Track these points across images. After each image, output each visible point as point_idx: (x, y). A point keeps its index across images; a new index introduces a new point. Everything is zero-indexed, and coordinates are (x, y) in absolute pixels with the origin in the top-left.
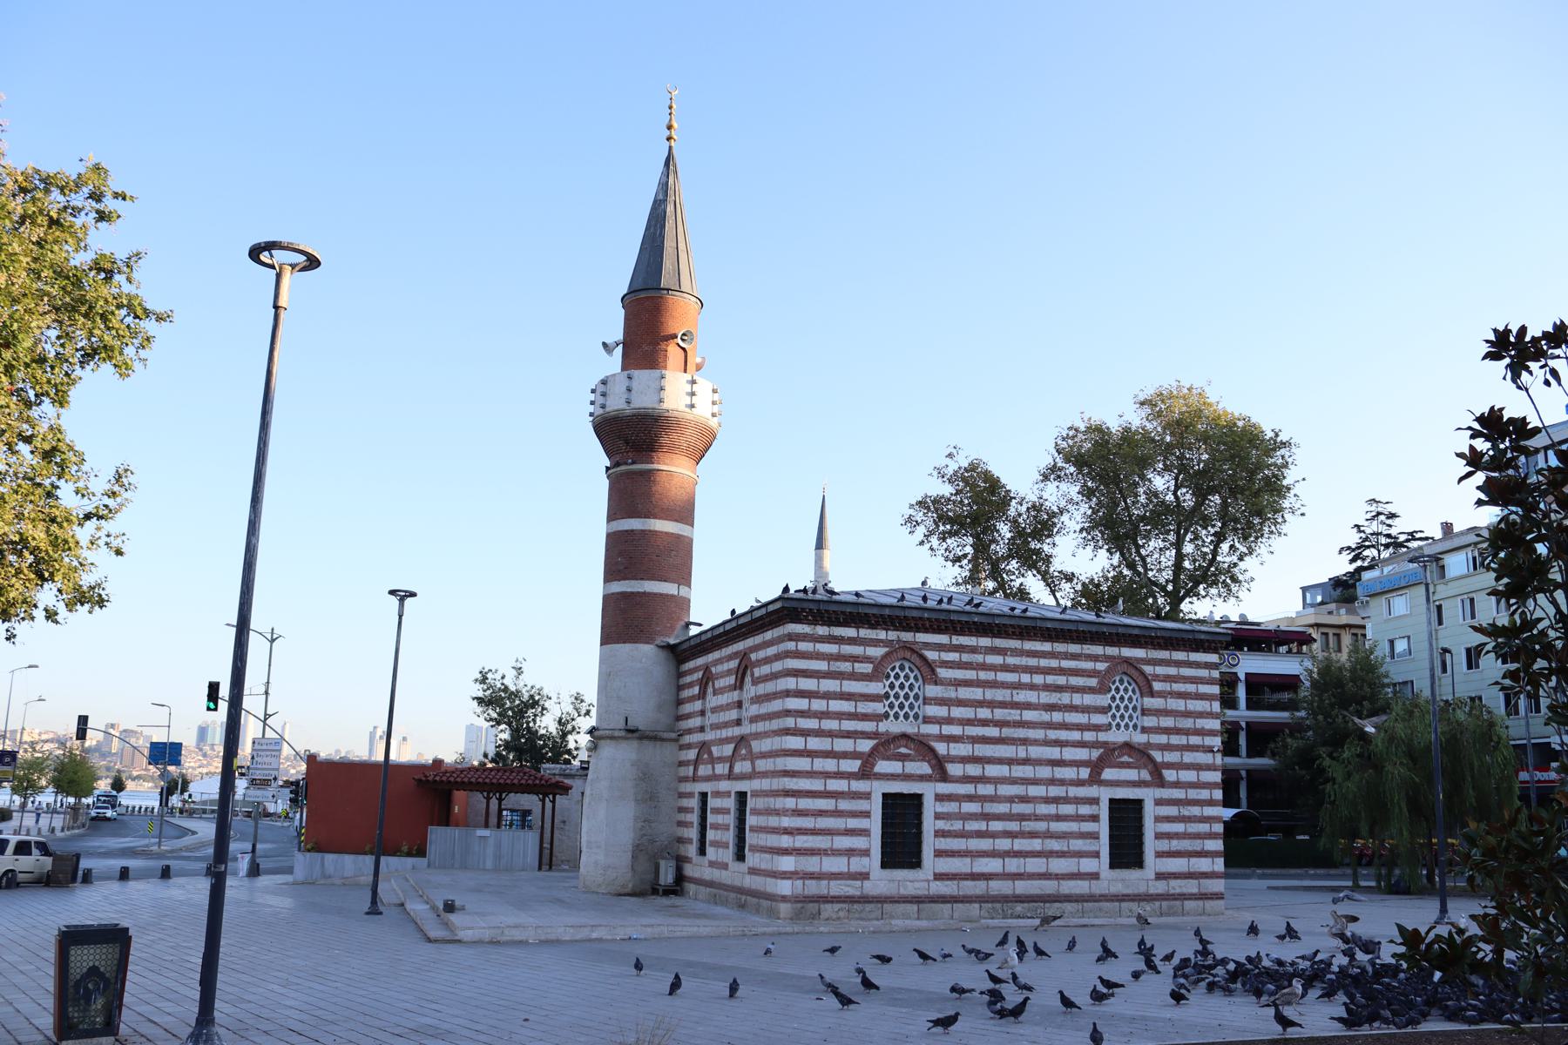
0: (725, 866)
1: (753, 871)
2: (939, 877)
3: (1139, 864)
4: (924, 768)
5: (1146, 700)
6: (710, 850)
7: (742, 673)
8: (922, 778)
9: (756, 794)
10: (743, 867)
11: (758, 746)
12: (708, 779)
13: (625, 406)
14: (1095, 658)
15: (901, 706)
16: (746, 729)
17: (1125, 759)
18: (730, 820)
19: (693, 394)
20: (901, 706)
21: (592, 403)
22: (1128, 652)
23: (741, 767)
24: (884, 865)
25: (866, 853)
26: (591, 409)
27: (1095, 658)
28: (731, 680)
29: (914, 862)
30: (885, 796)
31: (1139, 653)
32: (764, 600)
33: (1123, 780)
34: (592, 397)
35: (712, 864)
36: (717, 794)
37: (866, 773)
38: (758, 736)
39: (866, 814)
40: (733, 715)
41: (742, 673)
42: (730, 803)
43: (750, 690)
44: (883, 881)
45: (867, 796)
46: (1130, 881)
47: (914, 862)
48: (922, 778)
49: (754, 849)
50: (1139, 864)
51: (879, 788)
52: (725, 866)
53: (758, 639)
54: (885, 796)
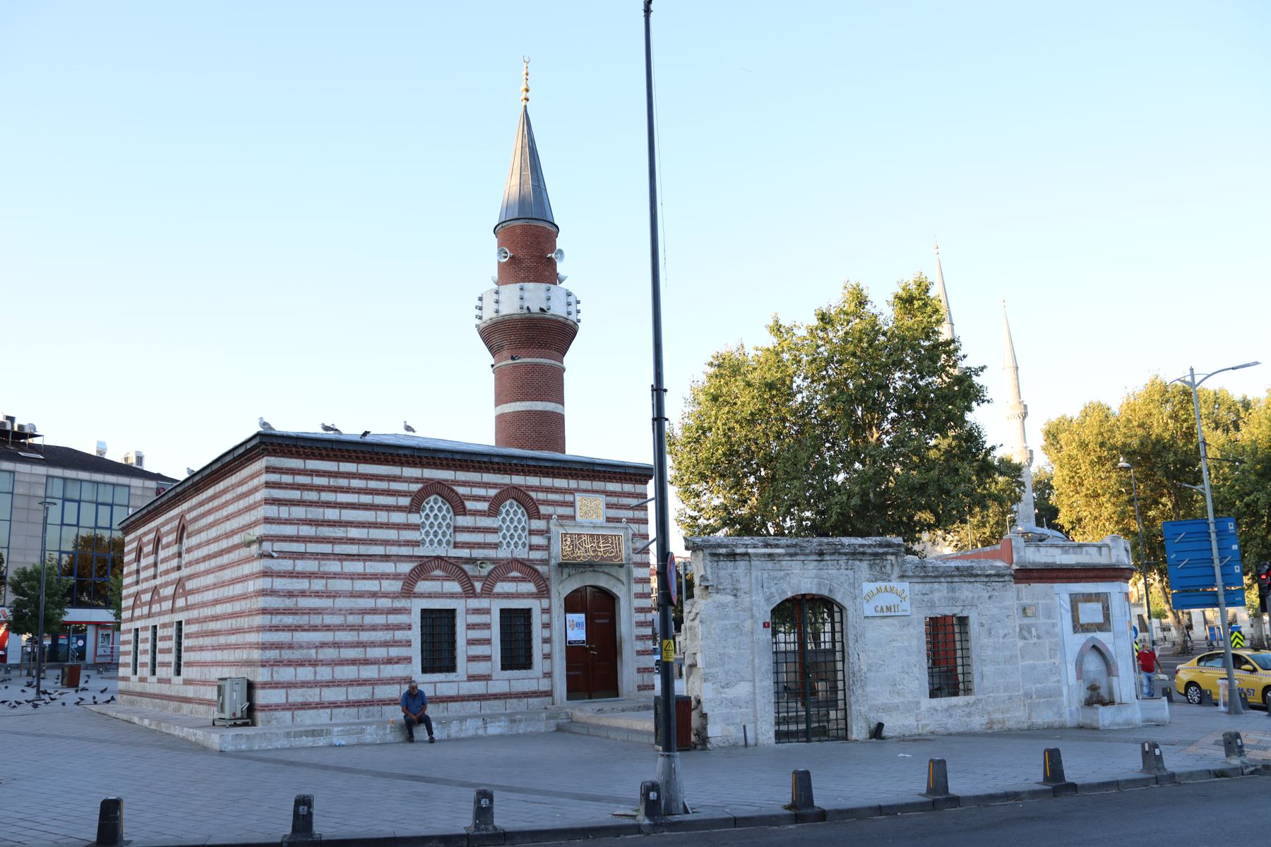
0: (168, 681)
1: (187, 682)
2: (471, 678)
3: (452, 668)
4: (455, 587)
5: (533, 521)
6: (158, 669)
7: (181, 531)
8: (452, 596)
9: (189, 622)
10: (154, 679)
11: (190, 585)
12: (183, 609)
13: (495, 315)
14: (487, 485)
15: (436, 534)
16: (185, 572)
17: (438, 573)
18: (172, 644)
19: (497, 302)
20: (436, 534)
21: (578, 312)
22: (518, 480)
23: (180, 602)
24: (505, 667)
25: (408, 660)
26: (478, 322)
27: (487, 485)
28: (172, 537)
29: (527, 664)
30: (502, 610)
31: (533, 481)
32: (196, 469)
33: (440, 592)
34: (579, 307)
35: (160, 681)
36: (189, 622)
37: (408, 592)
38: (190, 577)
39: (487, 626)
40: (175, 563)
41: (181, 531)
42: (172, 631)
43: (187, 543)
44: (504, 681)
45: (406, 611)
46: (520, 680)
47: (527, 664)
48: (452, 596)
49: (189, 664)
50: (452, 668)
51: (418, 605)
52: (168, 681)
53: (547, 482)
54: (502, 610)
